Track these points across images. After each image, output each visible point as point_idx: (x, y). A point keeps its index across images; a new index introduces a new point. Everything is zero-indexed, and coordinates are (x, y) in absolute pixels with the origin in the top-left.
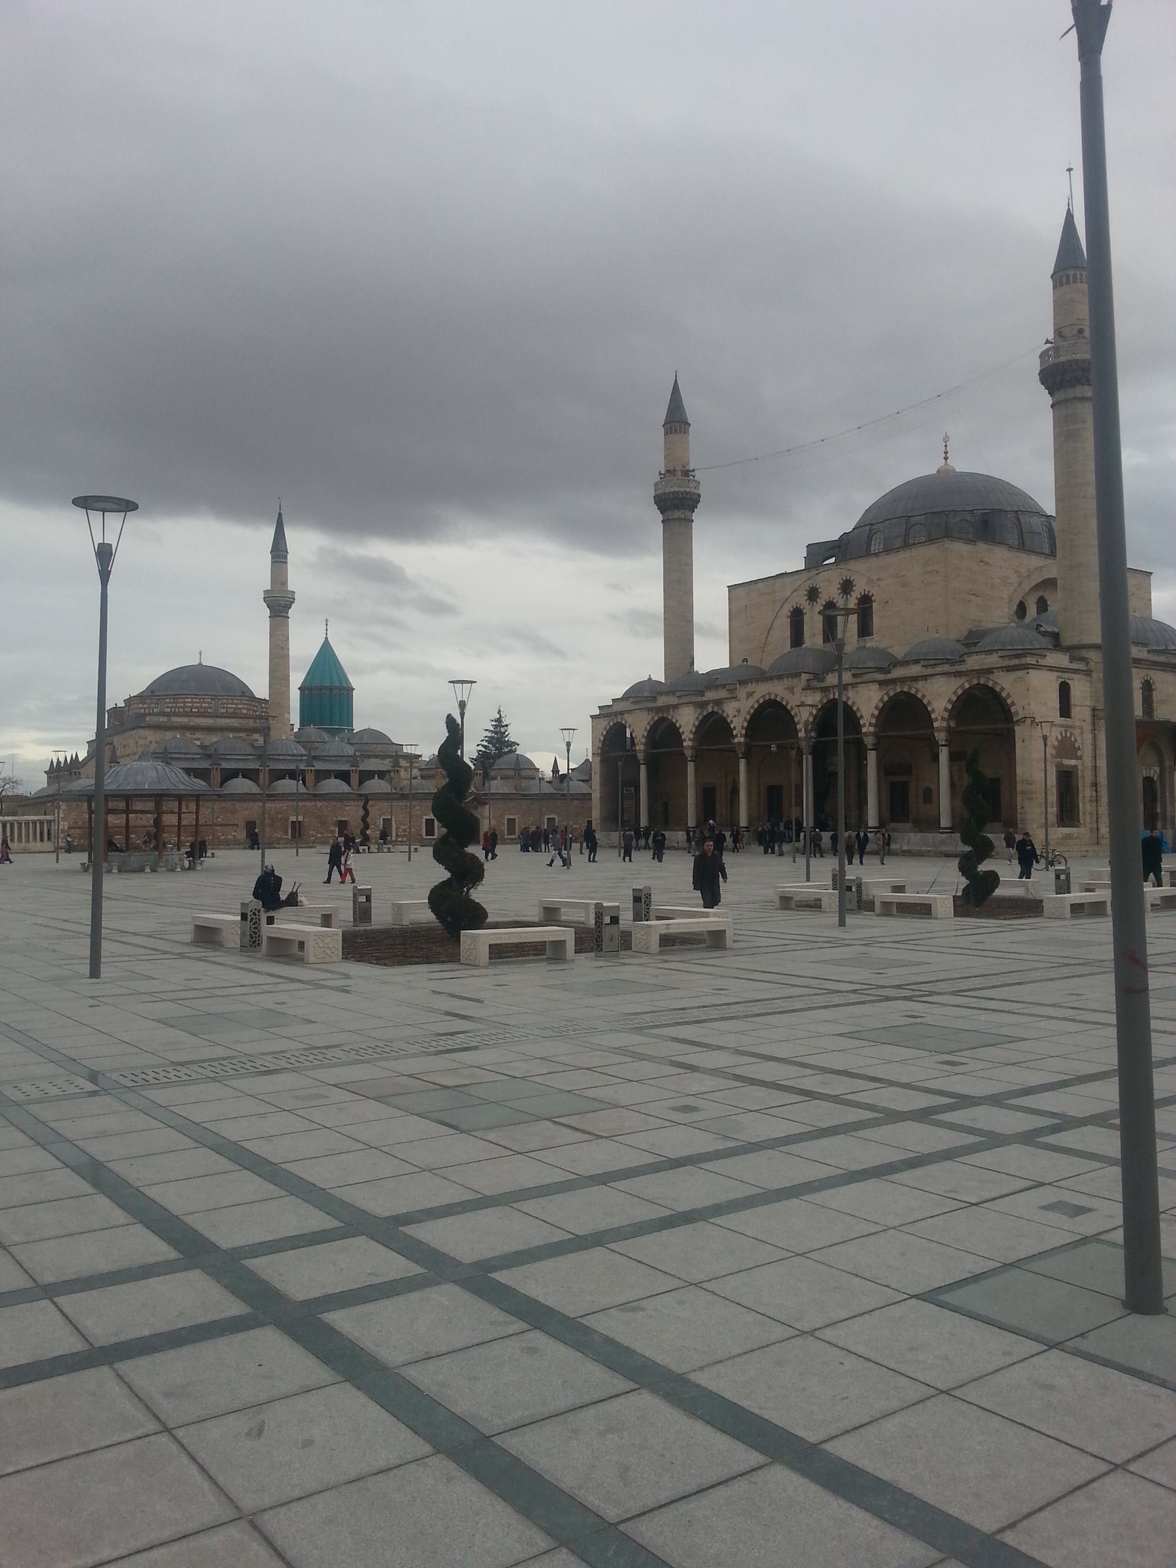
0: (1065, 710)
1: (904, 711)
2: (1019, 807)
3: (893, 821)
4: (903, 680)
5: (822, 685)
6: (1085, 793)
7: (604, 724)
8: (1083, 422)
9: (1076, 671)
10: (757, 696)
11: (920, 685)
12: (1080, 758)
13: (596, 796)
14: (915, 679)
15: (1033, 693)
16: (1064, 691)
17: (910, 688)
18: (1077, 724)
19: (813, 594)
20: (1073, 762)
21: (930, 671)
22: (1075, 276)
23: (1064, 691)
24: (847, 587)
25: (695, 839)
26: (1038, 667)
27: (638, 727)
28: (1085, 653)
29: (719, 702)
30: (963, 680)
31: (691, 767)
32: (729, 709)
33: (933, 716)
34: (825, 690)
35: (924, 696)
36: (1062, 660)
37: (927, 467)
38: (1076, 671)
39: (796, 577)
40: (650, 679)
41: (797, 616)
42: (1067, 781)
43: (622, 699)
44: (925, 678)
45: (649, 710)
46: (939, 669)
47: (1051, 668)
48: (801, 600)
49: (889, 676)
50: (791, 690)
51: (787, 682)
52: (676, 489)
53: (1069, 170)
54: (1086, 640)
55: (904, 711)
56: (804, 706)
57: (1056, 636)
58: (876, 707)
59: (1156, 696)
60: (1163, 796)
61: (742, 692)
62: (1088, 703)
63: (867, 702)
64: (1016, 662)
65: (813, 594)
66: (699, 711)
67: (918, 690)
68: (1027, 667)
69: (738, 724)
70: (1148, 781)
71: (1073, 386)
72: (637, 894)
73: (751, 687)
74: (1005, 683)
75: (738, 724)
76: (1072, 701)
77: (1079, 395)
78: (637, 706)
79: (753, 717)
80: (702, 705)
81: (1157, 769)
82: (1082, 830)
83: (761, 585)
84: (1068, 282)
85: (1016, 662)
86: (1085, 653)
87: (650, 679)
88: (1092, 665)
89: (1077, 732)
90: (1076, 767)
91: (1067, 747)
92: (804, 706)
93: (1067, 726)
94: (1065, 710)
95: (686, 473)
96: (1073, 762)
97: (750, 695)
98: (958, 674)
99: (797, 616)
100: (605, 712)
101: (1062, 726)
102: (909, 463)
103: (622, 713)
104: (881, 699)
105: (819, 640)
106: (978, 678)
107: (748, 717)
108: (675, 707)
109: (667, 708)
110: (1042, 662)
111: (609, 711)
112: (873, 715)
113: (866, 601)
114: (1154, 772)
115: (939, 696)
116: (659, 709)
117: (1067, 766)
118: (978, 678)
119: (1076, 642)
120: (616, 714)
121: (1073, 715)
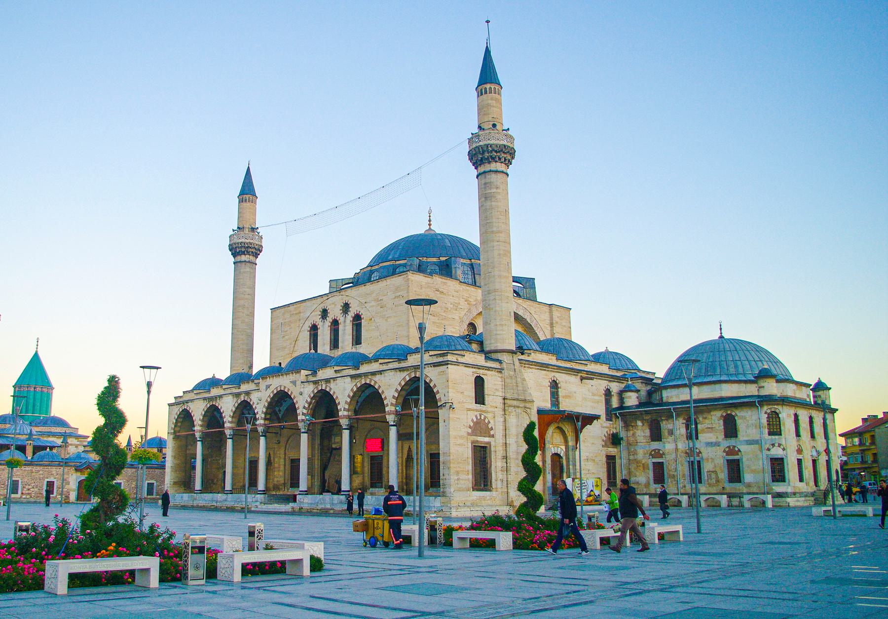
0: (480, 398)
1: (368, 399)
2: (441, 474)
3: (372, 487)
4: (366, 375)
5: (315, 379)
6: (496, 464)
7: (177, 410)
8: (497, 188)
9: (489, 369)
10: (272, 388)
11: (377, 378)
12: (493, 436)
13: (169, 463)
14: (374, 374)
15: (454, 382)
16: (479, 383)
17: (371, 380)
18: (490, 409)
19: (324, 313)
20: (486, 439)
21: (385, 367)
22: (490, 88)
23: (479, 383)
24: (346, 307)
25: (520, 524)
26: (457, 363)
27: (198, 410)
28: (499, 356)
29: (248, 393)
30: (406, 373)
31: (229, 443)
32: (254, 398)
33: (385, 402)
34: (316, 383)
35: (380, 387)
36: (480, 359)
37: (420, 229)
38: (489, 369)
39: (314, 301)
40: (214, 377)
41: (314, 328)
42: (481, 455)
43: (192, 391)
44: (380, 372)
45: (205, 399)
46: (391, 366)
47: (467, 365)
48: (317, 319)
49: (358, 372)
50: (294, 383)
51: (292, 377)
52: (243, 240)
53: (488, 22)
54: (500, 347)
55: (368, 399)
56: (303, 396)
57: (481, 343)
58: (349, 396)
59: (561, 393)
60: (568, 469)
61: (263, 384)
62: (501, 394)
63: (343, 391)
64: (441, 359)
65: (324, 313)
66: (235, 399)
67: (376, 382)
68: (446, 363)
69: (260, 409)
70: (556, 456)
71: (489, 163)
72: (247, 548)
73: (269, 381)
74: (432, 375)
75: (260, 409)
76: (486, 392)
77: (494, 169)
78: (198, 397)
79: (270, 404)
80: (237, 395)
81: (563, 448)
82: (494, 493)
83: (291, 308)
84: (486, 93)
85: (441, 359)
86: (499, 356)
87: (214, 377)
88: (504, 365)
89: (489, 416)
90: (489, 443)
91: (480, 427)
92: (303, 396)
93: (481, 411)
94: (480, 398)
95: (253, 229)
96: (486, 439)
97: (268, 387)
98: (401, 369)
99: (314, 328)
100: (179, 401)
101: (477, 411)
102: (414, 227)
103: (187, 402)
104: (352, 390)
105: (327, 347)
106: (415, 372)
107: (266, 404)
108: (221, 397)
109: (215, 398)
110: (461, 360)
111: (181, 400)
112: (346, 402)
113: (357, 318)
114: (561, 450)
115: (389, 385)
116: (211, 399)
117: (481, 442)
118: (415, 372)
119: (493, 348)
120: (184, 403)
121: (486, 402)
